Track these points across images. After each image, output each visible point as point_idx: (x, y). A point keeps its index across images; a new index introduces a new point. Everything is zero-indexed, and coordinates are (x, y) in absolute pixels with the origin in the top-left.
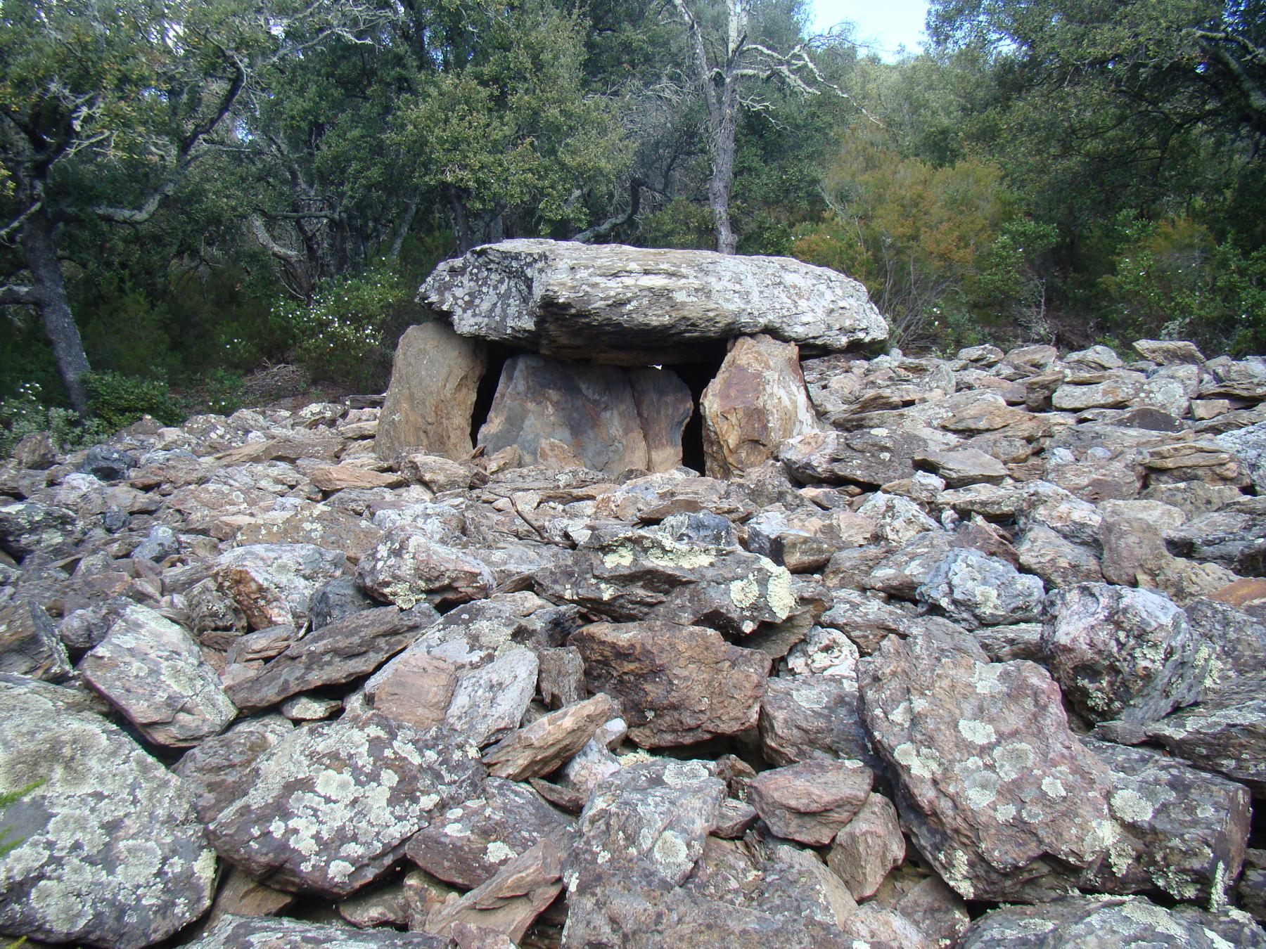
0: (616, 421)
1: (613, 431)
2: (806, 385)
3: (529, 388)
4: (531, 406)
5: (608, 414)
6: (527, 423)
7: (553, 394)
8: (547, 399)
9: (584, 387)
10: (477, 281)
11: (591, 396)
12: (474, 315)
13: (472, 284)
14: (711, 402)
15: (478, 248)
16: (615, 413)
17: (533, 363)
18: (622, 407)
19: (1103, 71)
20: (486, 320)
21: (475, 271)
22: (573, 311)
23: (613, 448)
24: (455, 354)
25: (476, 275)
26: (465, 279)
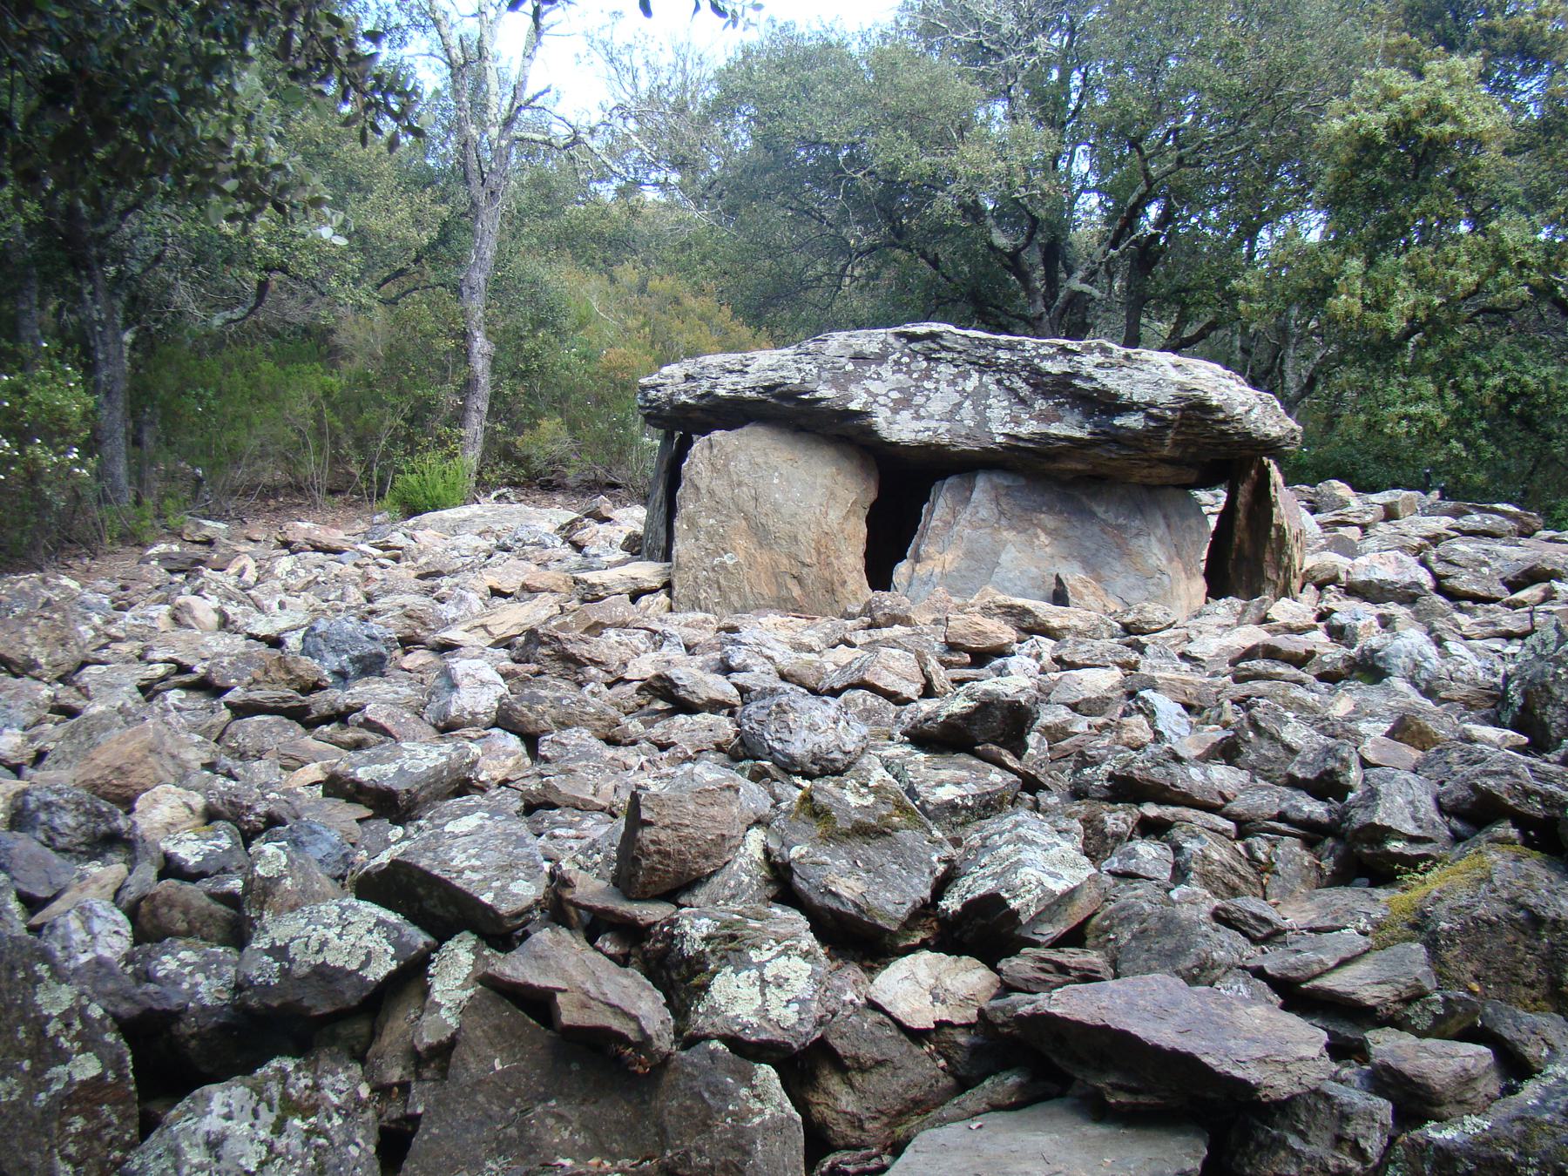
0: (1156, 548)
1: (1153, 561)
2: (1158, 736)
3: (1002, 513)
4: (1008, 535)
5: (1142, 541)
6: (1004, 558)
7: (1048, 520)
8: (1038, 526)
9: (1096, 508)
10: (909, 373)
11: (1112, 521)
12: (918, 417)
13: (900, 376)
14: (354, 967)
15: (921, 329)
16: (1153, 539)
17: (1000, 480)
18: (1159, 532)
19: (1509, 414)
20: (946, 425)
21: (905, 360)
22: (1221, 416)
23: (1155, 581)
24: (830, 470)
25: (908, 365)
26: (886, 370)
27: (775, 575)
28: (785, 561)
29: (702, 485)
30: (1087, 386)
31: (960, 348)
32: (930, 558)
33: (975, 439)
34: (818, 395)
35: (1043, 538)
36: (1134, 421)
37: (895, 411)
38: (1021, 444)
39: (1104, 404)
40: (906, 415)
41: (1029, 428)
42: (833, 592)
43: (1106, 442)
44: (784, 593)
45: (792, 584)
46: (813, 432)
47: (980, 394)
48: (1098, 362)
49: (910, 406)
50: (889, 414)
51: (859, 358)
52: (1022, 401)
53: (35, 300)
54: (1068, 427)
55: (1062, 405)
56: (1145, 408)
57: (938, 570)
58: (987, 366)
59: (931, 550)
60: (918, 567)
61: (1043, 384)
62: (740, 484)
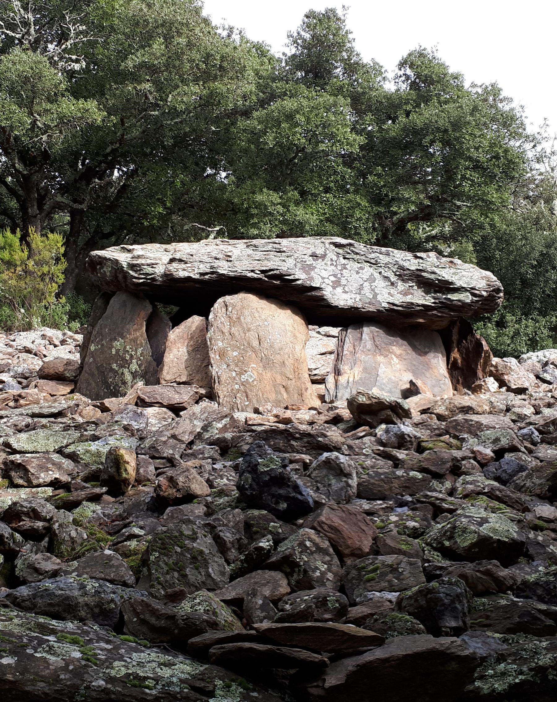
27: (275, 386)
28: (279, 377)
29: (226, 330)
30: (432, 277)
31: (362, 253)
32: (345, 372)
33: (373, 304)
34: (297, 277)
35: (396, 360)
36: (467, 298)
37: (334, 288)
38: (395, 308)
39: (445, 287)
40: (339, 290)
41: (398, 299)
42: (301, 395)
43: (440, 307)
44: (279, 397)
45: (283, 390)
46: (273, 298)
47: (371, 279)
48: (431, 263)
49: (340, 285)
50: (331, 289)
51: (314, 256)
52: (392, 284)
53: (528, 146)
54: (420, 298)
55: (412, 286)
56: (472, 291)
57: (351, 380)
58: (375, 264)
59: (346, 368)
60: (340, 378)
61: (404, 275)
62: (249, 330)
